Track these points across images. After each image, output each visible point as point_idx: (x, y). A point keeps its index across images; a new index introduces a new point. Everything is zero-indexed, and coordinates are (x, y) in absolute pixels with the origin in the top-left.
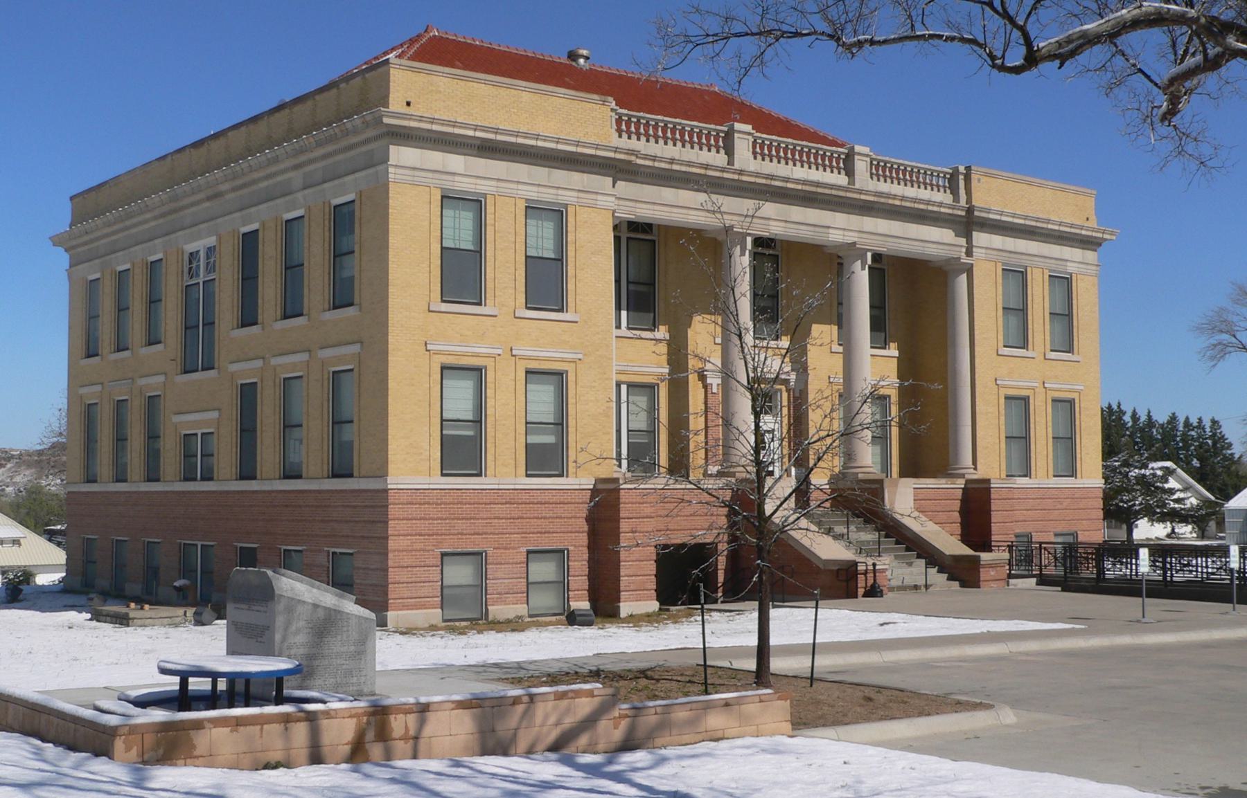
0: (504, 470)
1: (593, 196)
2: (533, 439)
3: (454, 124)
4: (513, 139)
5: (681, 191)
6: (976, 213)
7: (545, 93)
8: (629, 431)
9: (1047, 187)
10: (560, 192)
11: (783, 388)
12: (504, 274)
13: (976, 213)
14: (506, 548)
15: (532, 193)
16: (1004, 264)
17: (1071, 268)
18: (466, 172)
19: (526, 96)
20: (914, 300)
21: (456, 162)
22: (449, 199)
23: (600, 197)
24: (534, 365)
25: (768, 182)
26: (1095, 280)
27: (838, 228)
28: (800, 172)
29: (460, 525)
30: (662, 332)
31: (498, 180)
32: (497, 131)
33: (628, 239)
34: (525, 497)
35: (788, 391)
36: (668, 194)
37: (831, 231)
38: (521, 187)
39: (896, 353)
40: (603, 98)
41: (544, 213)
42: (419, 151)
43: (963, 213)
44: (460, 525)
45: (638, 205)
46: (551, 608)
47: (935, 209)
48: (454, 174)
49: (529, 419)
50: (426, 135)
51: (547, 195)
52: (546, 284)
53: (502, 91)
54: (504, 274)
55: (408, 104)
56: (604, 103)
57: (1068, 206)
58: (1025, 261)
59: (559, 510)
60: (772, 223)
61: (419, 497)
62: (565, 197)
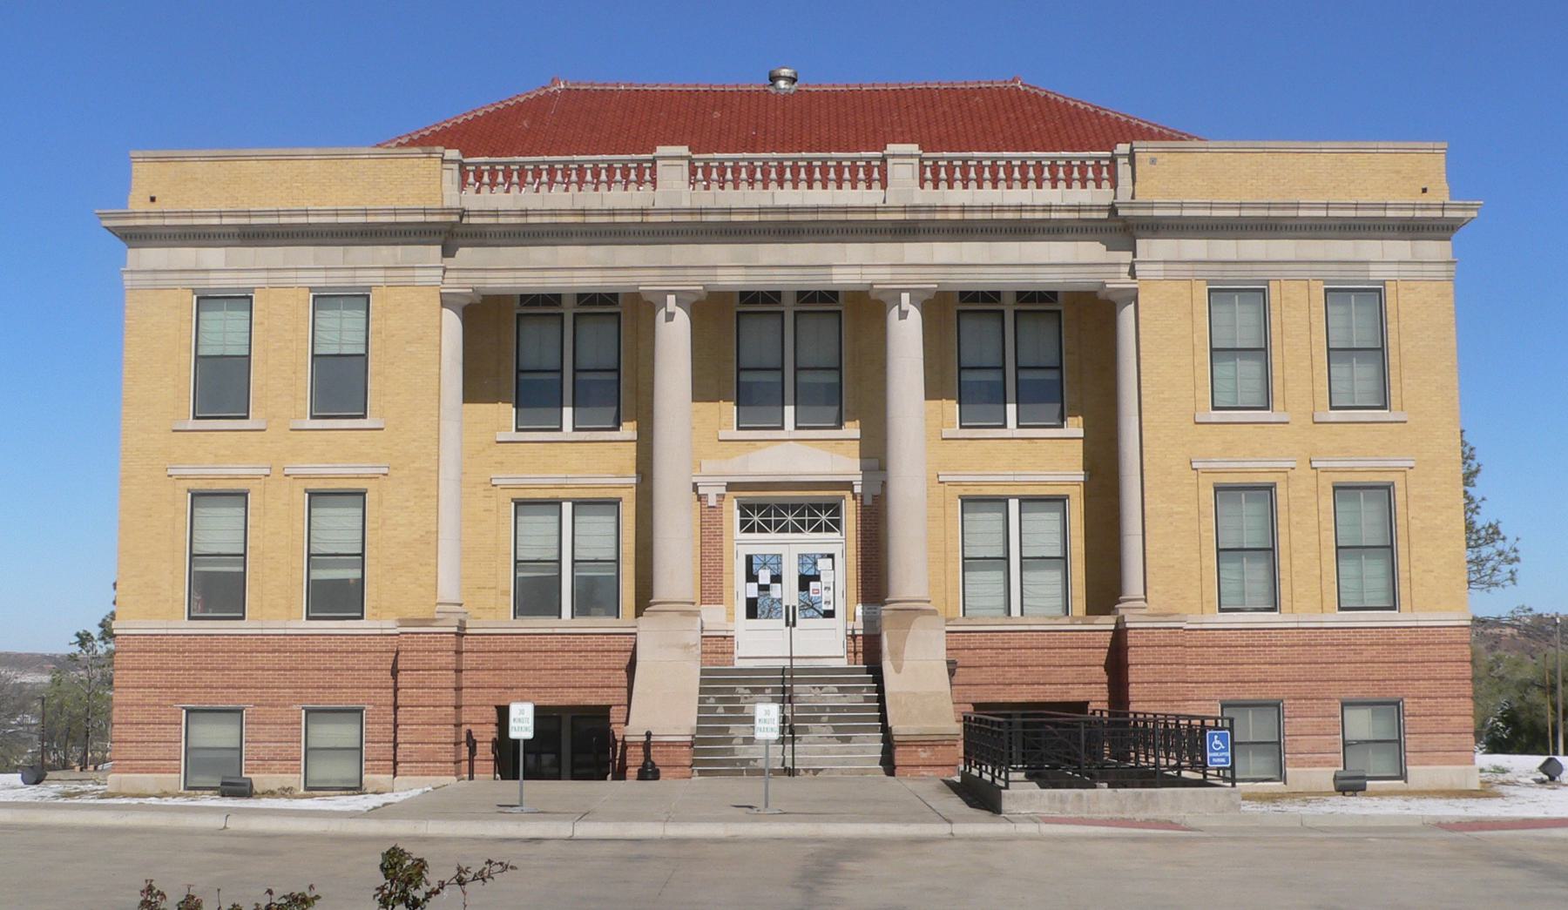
0: (276, 608)
1: (410, 272)
2: (319, 574)
3: (192, 214)
4: (274, 220)
5: (561, 249)
6: (1121, 213)
7: (341, 157)
8: (574, 561)
9: (1320, 151)
10: (359, 273)
11: (848, 494)
12: (282, 381)
13: (1121, 213)
14: (272, 706)
15: (319, 280)
16: (1209, 282)
17: (1377, 273)
18: (219, 265)
19: (200, 168)
20: (1040, 353)
21: (213, 256)
22: (1217, 293)
23: (418, 272)
24: (973, 491)
25: (726, 218)
26: (1450, 287)
27: (849, 266)
28: (819, 196)
29: (208, 677)
30: (852, 430)
31: (1400, 262)
32: (249, 214)
33: (796, 313)
34: (300, 644)
35: (855, 497)
36: (540, 254)
37: (834, 270)
38: (300, 274)
39: (856, 434)
40: (428, 149)
41: (341, 301)
42: (1205, 242)
43: (1105, 215)
44: (208, 677)
45: (488, 275)
46: (347, 781)
47: (1039, 215)
48: (715, 267)
49: (522, 555)
50: (1294, 222)
51: (340, 279)
52: (340, 386)
53: (280, 164)
54: (282, 381)
55: (153, 199)
56: (429, 155)
57: (1403, 175)
58: (1260, 273)
59: (352, 661)
60: (719, 272)
61: (154, 644)
62: (364, 278)
